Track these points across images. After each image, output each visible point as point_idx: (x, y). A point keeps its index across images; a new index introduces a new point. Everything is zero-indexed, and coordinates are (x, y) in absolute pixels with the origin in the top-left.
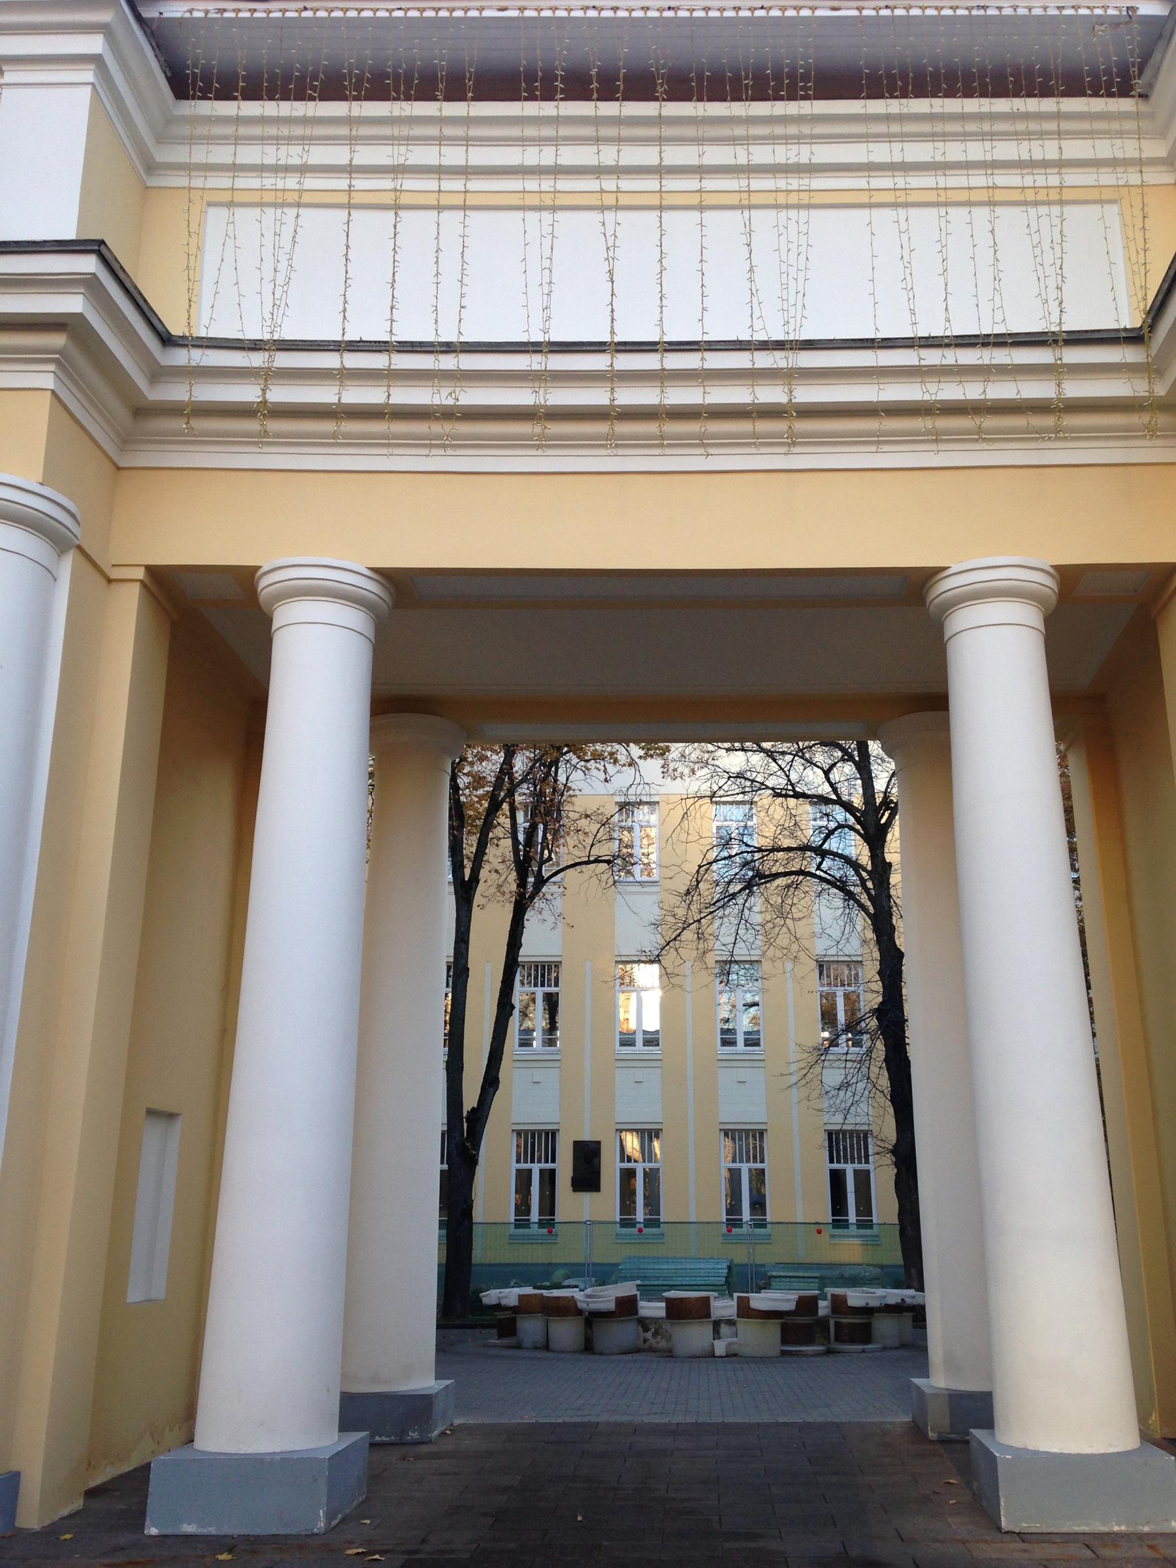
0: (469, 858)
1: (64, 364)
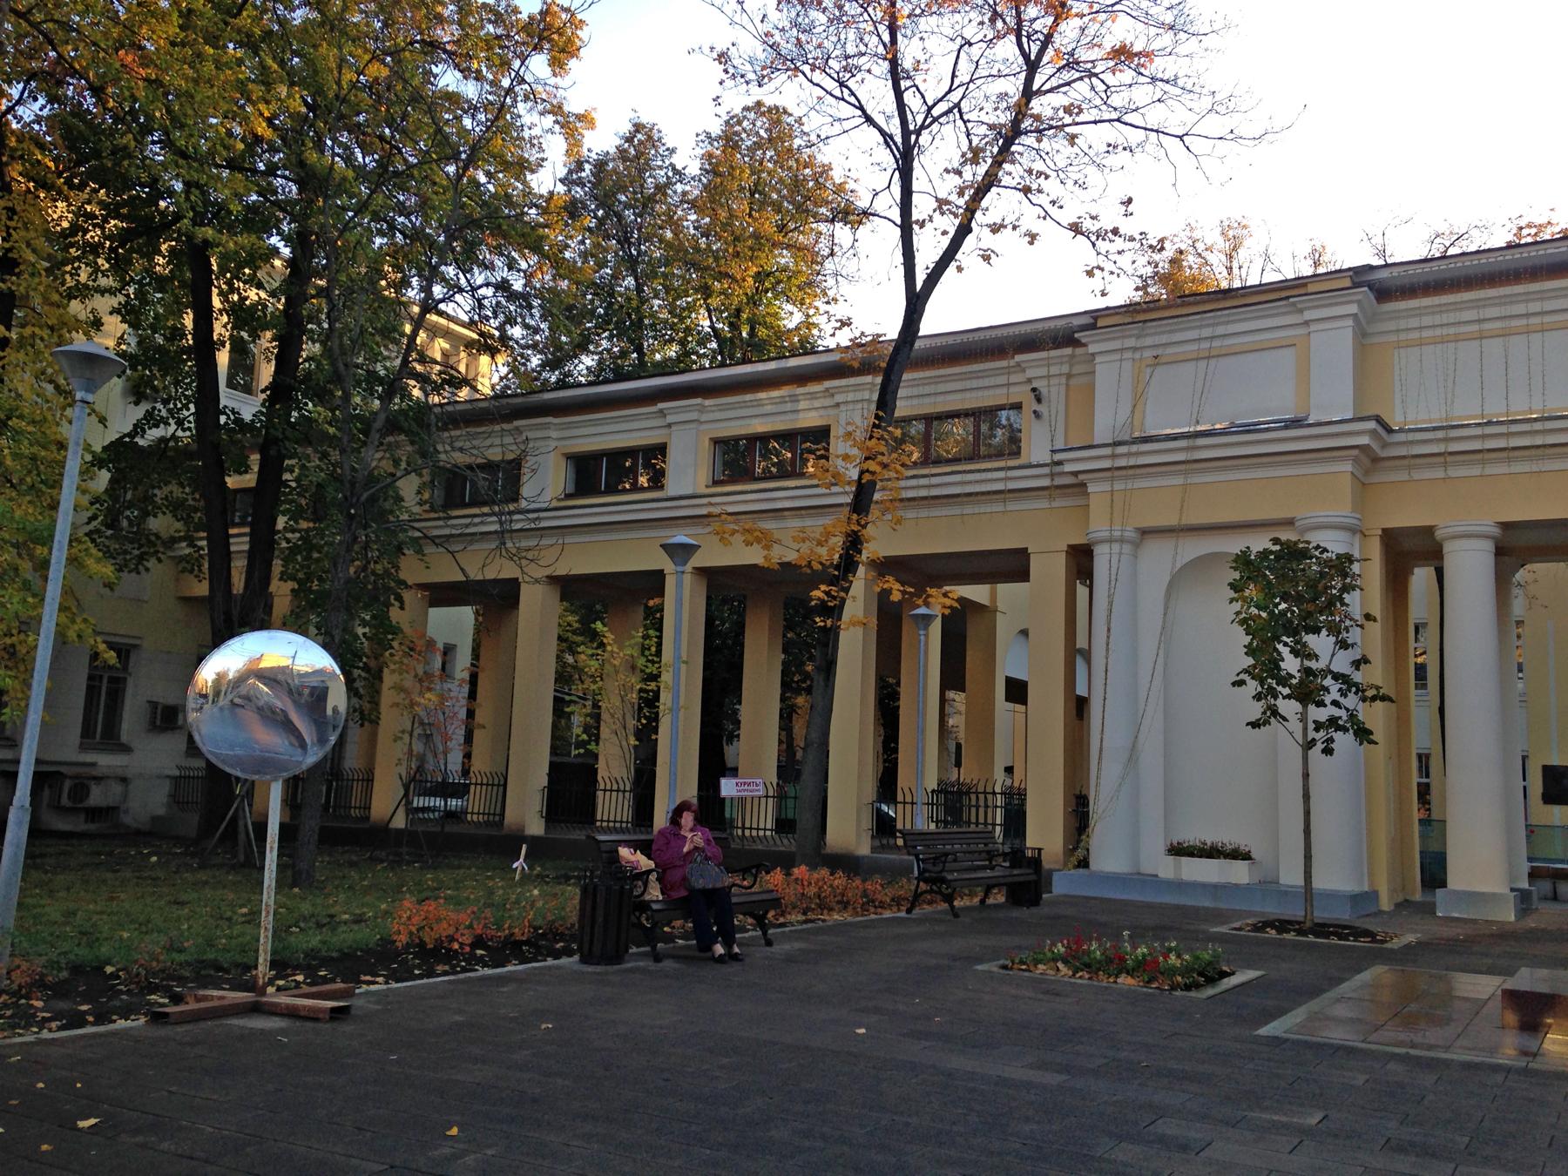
1: (1356, 460)
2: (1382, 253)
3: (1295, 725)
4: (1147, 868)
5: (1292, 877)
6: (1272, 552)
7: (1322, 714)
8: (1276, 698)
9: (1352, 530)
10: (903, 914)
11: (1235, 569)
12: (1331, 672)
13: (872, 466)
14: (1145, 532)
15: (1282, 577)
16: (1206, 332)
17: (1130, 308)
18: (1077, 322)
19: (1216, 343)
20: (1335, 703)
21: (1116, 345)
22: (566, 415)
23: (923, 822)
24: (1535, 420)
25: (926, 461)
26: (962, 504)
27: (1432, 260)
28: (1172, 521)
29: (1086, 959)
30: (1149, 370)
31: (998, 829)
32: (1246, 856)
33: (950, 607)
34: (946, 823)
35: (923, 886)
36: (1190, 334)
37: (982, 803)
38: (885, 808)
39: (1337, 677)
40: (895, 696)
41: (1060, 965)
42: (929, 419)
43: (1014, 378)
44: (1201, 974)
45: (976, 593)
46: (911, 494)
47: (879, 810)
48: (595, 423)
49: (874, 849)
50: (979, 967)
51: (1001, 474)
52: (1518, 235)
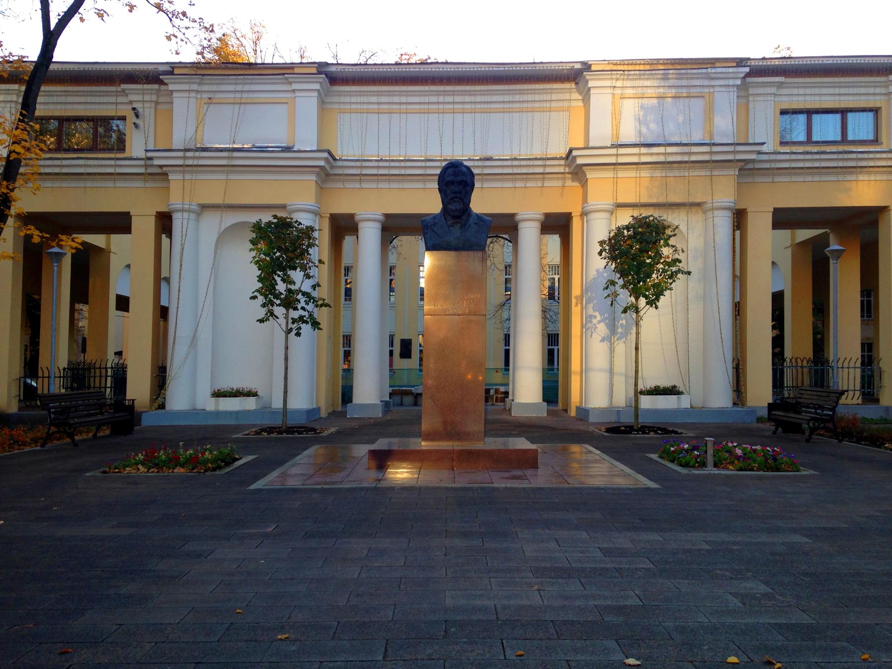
0: (284, 476)
1: (318, 174)
3: (282, 321)
4: (200, 405)
5: (277, 404)
6: (273, 223)
7: (295, 314)
8: (272, 305)
9: (315, 213)
10: (38, 448)
11: (253, 232)
12: (301, 291)
13: (18, 148)
14: (204, 207)
15: (278, 238)
16: (239, 88)
17: (195, 65)
18: (162, 68)
19: (245, 95)
20: (303, 308)
21: (185, 87)
23: (57, 387)
24: (402, 161)
25: (59, 148)
26: (86, 180)
27: (360, 64)
28: (218, 200)
29: (156, 461)
30: (206, 106)
31: (108, 390)
32: (255, 395)
33: (76, 248)
34: (72, 388)
35: (53, 429)
36: (229, 87)
37: (98, 374)
38: (29, 381)
39: (304, 294)
40: (38, 307)
41: (140, 467)
42: (62, 120)
43: (121, 99)
44: (222, 461)
45: (97, 240)
46: (47, 170)
47: (25, 383)
49: (20, 409)
50: (88, 474)
51: (112, 162)
52: (401, 59)
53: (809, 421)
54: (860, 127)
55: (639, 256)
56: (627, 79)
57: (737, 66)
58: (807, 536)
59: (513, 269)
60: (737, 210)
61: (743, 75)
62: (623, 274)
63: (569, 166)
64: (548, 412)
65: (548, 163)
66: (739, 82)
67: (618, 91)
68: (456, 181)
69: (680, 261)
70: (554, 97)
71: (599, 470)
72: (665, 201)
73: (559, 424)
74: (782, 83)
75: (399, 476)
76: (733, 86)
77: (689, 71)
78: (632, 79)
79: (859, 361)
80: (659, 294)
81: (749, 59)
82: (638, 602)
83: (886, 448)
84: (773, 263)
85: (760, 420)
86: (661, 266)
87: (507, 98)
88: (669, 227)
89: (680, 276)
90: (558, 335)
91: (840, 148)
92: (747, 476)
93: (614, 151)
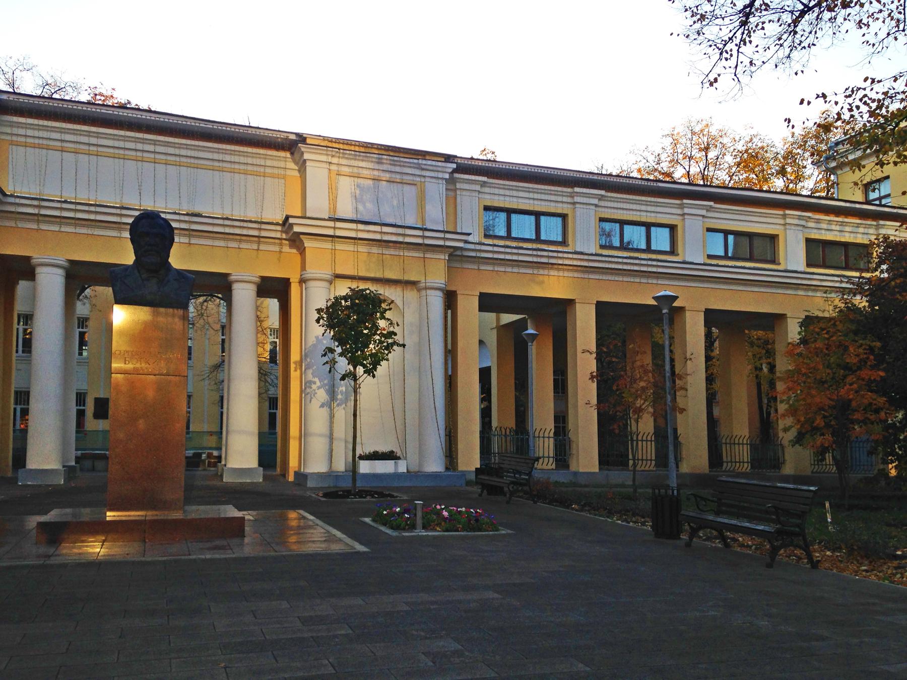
2: (12, 85)
22: (536, 183)
24: (91, 205)
27: (44, 97)
48: (761, 215)
53: (509, 484)
54: (551, 229)
55: (356, 325)
56: (343, 158)
57: (445, 161)
58: (498, 592)
59: (226, 331)
60: (447, 291)
61: (450, 170)
62: (342, 343)
63: (286, 232)
64: (265, 477)
65: (264, 226)
66: (447, 176)
67: (333, 167)
68: (152, 233)
69: (395, 334)
70: (269, 163)
71: (317, 536)
72: (381, 276)
73: (278, 487)
74: (485, 182)
75: (91, 550)
76: (442, 179)
77: (402, 159)
78: (347, 158)
79: (553, 431)
80: (376, 363)
81: (456, 157)
82: (331, 670)
83: (573, 509)
84: (481, 342)
85: (469, 483)
86: (378, 337)
87: (216, 156)
88: (385, 301)
89: (395, 347)
90: (277, 398)
91: (535, 246)
92: (452, 536)
93: (331, 224)
